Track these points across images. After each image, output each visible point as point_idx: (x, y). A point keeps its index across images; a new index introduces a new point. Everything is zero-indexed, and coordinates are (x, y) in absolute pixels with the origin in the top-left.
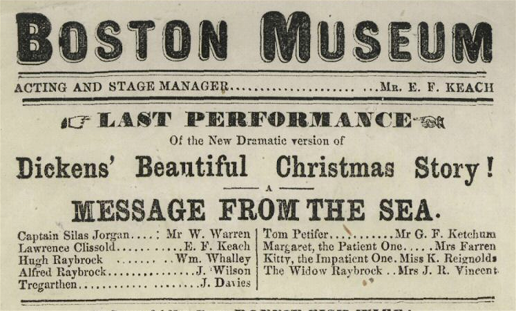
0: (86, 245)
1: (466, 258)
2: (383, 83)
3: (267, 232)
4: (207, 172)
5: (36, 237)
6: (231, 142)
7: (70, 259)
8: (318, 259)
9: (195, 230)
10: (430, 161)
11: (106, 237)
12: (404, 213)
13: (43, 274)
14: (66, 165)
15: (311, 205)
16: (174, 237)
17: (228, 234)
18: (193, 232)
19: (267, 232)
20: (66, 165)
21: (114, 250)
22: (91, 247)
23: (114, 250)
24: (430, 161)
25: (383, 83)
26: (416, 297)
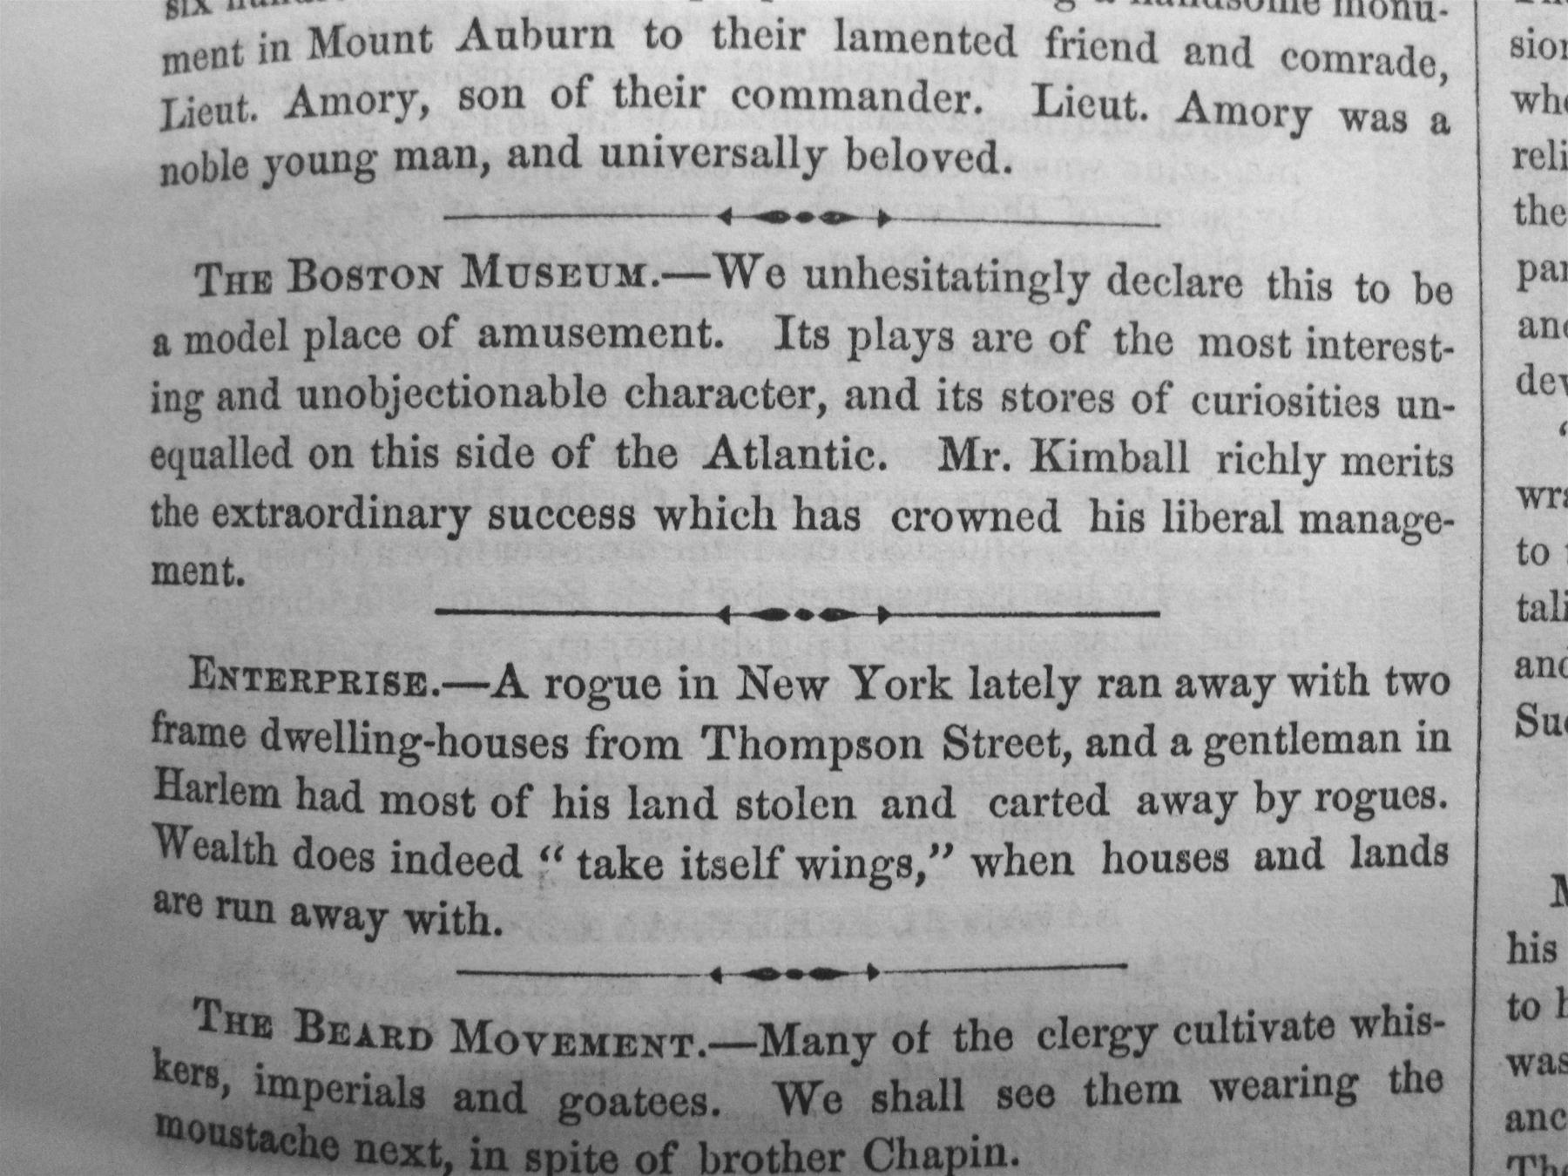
0: (360, 729)
1: (1371, 794)
2: (316, 31)
3: (208, 1011)
4: (633, 461)
5: (557, 1160)
6: (443, 277)
7: (919, 332)
8: (634, 810)
9: (739, 258)
10: (972, 733)
11: (723, 1166)
12: (202, 676)
13: (1142, 287)
14: (633, 860)
15: (711, 733)
16: (971, 467)
17: (203, 790)
18: (730, 261)
19: (208, 1011)
20: (633, 860)
21: (993, 169)
22: (351, 332)
23: (993, 169)
24: (972, 733)
25: (316, 31)
26: (588, 971)
